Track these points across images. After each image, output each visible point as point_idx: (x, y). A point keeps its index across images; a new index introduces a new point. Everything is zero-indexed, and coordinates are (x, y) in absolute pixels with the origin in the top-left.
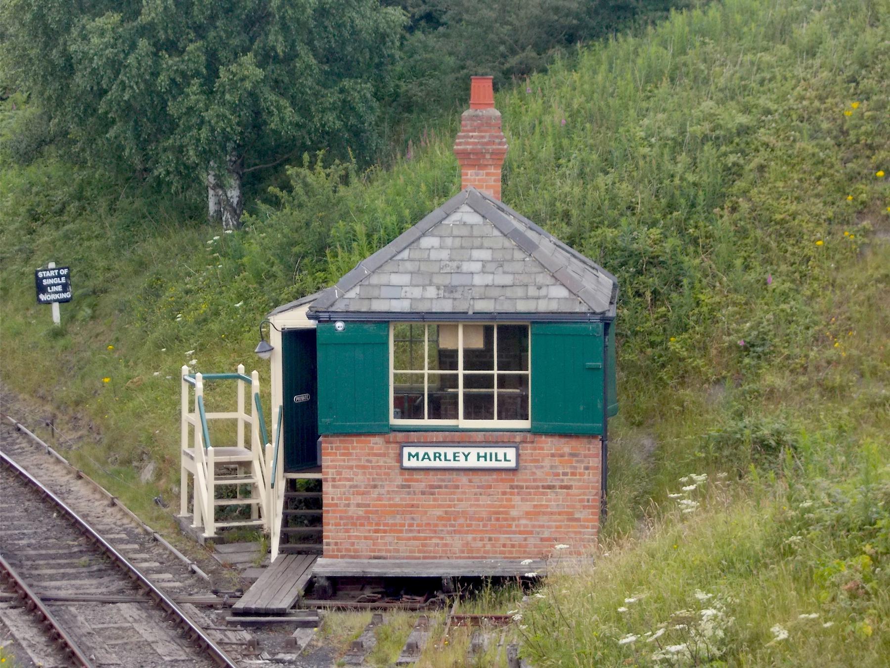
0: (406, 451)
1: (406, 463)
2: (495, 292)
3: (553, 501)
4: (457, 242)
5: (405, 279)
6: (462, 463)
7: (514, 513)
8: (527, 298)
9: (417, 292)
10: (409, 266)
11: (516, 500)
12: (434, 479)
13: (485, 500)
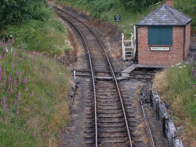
0: (151, 48)
1: (151, 49)
2: (166, 22)
3: (175, 56)
4: (161, 13)
5: (152, 19)
6: (160, 50)
7: (169, 58)
8: (171, 23)
9: (153, 22)
10: (153, 17)
11: (169, 56)
12: (156, 52)
13: (164, 56)
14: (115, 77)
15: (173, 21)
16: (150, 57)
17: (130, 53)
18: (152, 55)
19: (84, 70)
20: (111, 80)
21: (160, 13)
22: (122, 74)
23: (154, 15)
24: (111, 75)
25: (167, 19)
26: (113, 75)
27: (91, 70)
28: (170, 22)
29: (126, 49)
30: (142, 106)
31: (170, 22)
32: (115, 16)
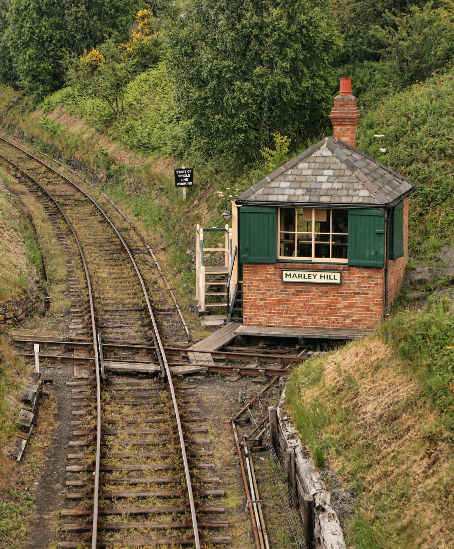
0: (284, 273)
1: (285, 279)
6: (312, 280)
7: (339, 306)
8: (348, 195)
9: (292, 192)
10: (291, 178)
12: (299, 288)
13: (324, 299)
14: (166, 365)
15: (355, 190)
16: (279, 303)
17: (220, 289)
18: (286, 297)
19: (71, 340)
20: (156, 374)
21: (313, 166)
22: (190, 355)
23: (295, 172)
24: (156, 361)
25: (337, 185)
26: (160, 360)
27: (92, 341)
28: (345, 192)
29: (208, 277)
30: (247, 459)
31: (345, 192)
32: (175, 171)
